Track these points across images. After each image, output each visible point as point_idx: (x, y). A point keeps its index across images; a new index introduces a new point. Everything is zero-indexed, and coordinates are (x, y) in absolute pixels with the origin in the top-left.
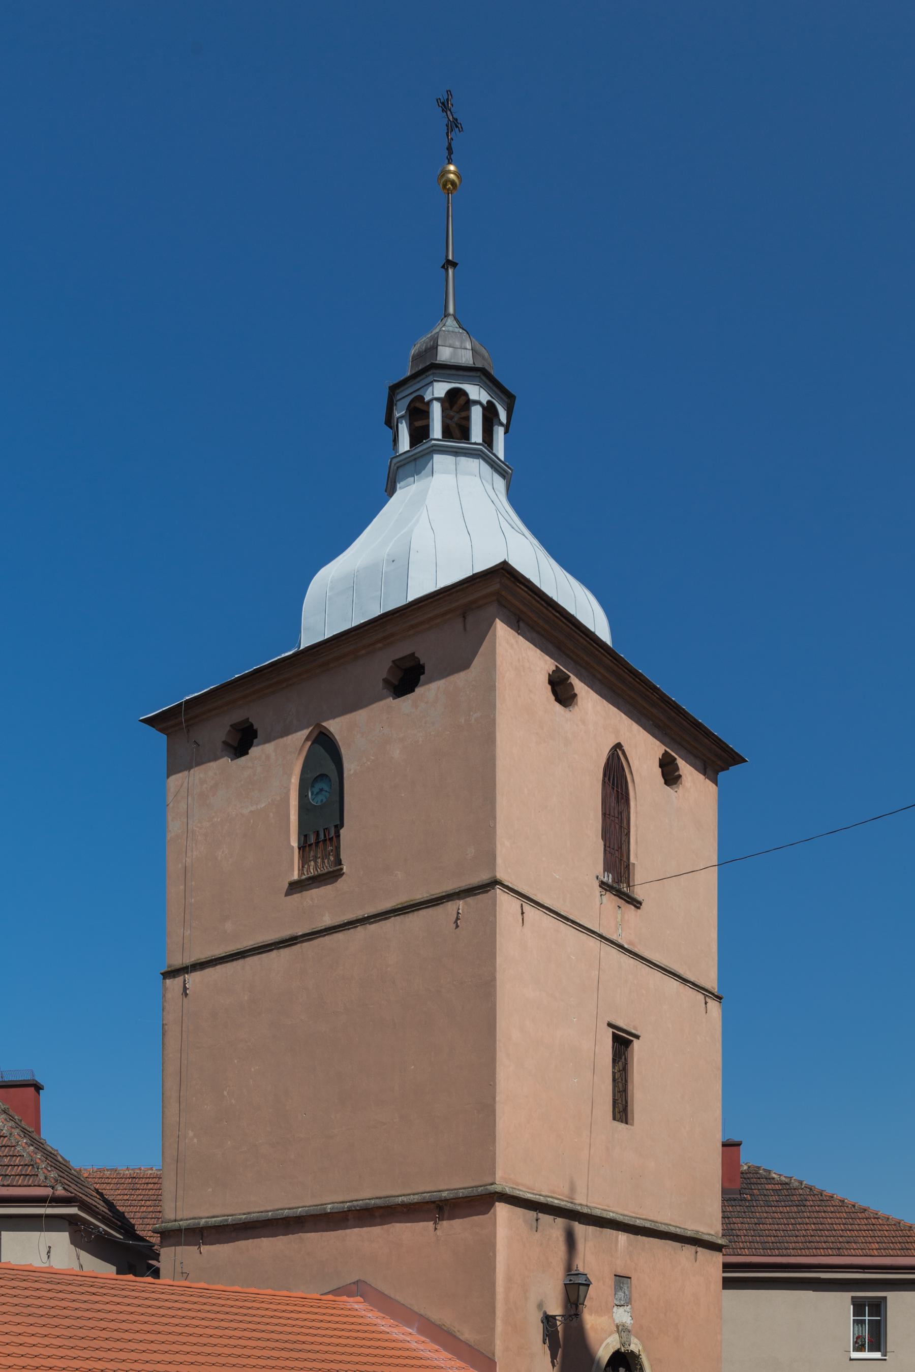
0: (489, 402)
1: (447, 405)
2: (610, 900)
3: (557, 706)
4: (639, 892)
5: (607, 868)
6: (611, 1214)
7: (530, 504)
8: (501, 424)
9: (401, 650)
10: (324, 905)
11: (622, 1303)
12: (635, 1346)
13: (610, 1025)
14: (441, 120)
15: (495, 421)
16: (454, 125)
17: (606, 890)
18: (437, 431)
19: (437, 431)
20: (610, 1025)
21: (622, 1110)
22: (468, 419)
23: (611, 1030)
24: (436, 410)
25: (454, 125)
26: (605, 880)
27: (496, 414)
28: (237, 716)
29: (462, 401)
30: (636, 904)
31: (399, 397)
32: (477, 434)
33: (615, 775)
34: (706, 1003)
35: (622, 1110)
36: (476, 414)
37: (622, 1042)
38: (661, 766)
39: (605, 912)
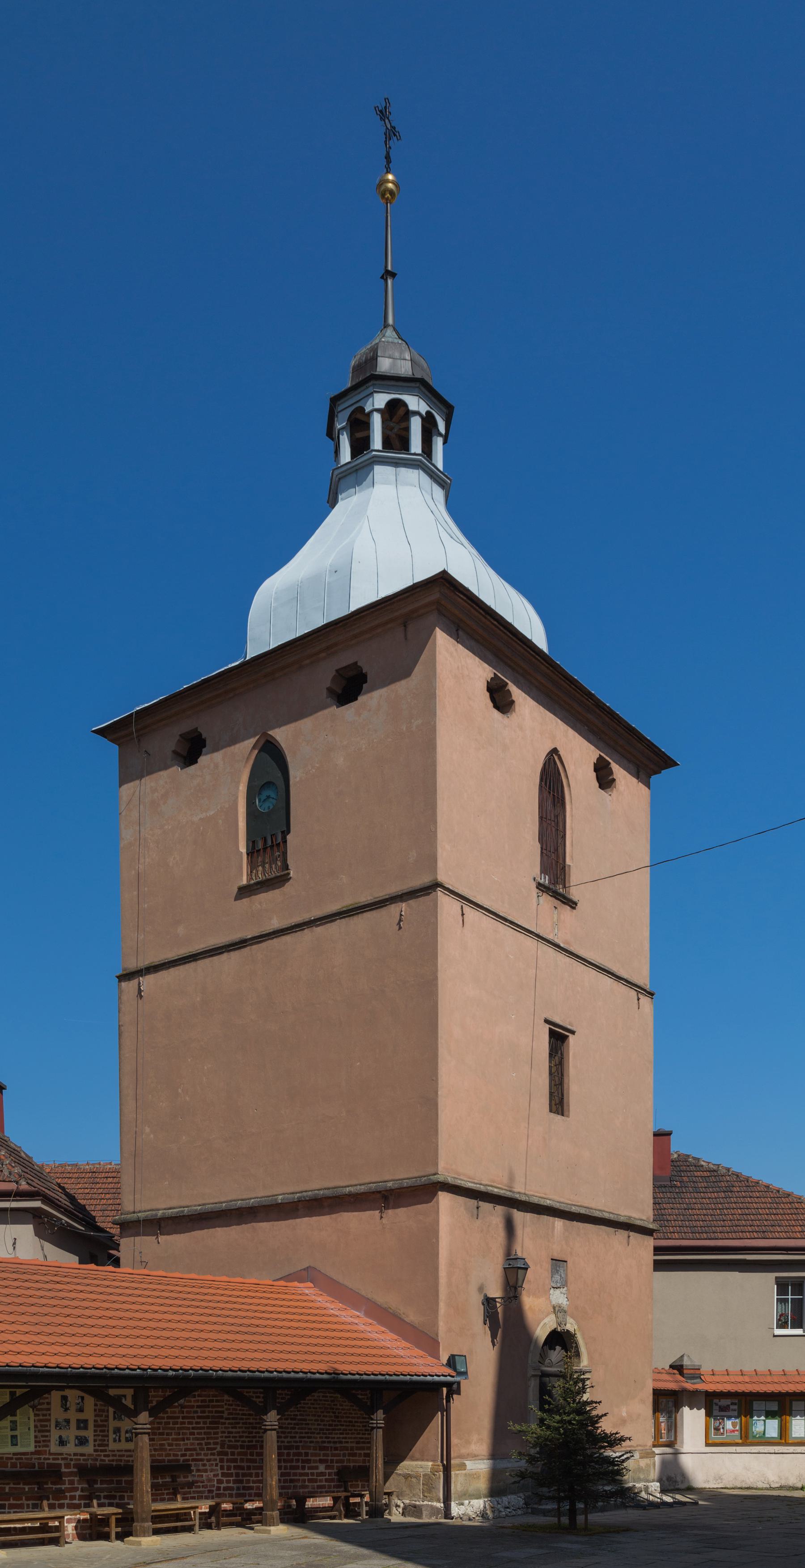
0: (428, 413)
1: (387, 416)
2: (547, 901)
3: (496, 714)
4: (574, 893)
5: (544, 870)
6: (548, 1202)
7: (470, 515)
8: (440, 435)
9: (345, 659)
10: (272, 909)
11: (559, 1285)
12: (571, 1326)
13: (547, 1021)
14: (379, 128)
15: (434, 431)
16: (391, 133)
17: (543, 891)
18: (377, 442)
19: (377, 442)
20: (547, 1021)
21: (558, 1102)
22: (407, 429)
23: (548, 1026)
24: (377, 421)
25: (391, 133)
26: (542, 881)
27: (435, 424)
28: (186, 726)
29: (401, 412)
30: (572, 904)
31: (340, 408)
32: (416, 446)
33: (552, 779)
34: (638, 999)
35: (558, 1102)
36: (416, 425)
37: (558, 1037)
38: (596, 770)
39: (542, 913)
